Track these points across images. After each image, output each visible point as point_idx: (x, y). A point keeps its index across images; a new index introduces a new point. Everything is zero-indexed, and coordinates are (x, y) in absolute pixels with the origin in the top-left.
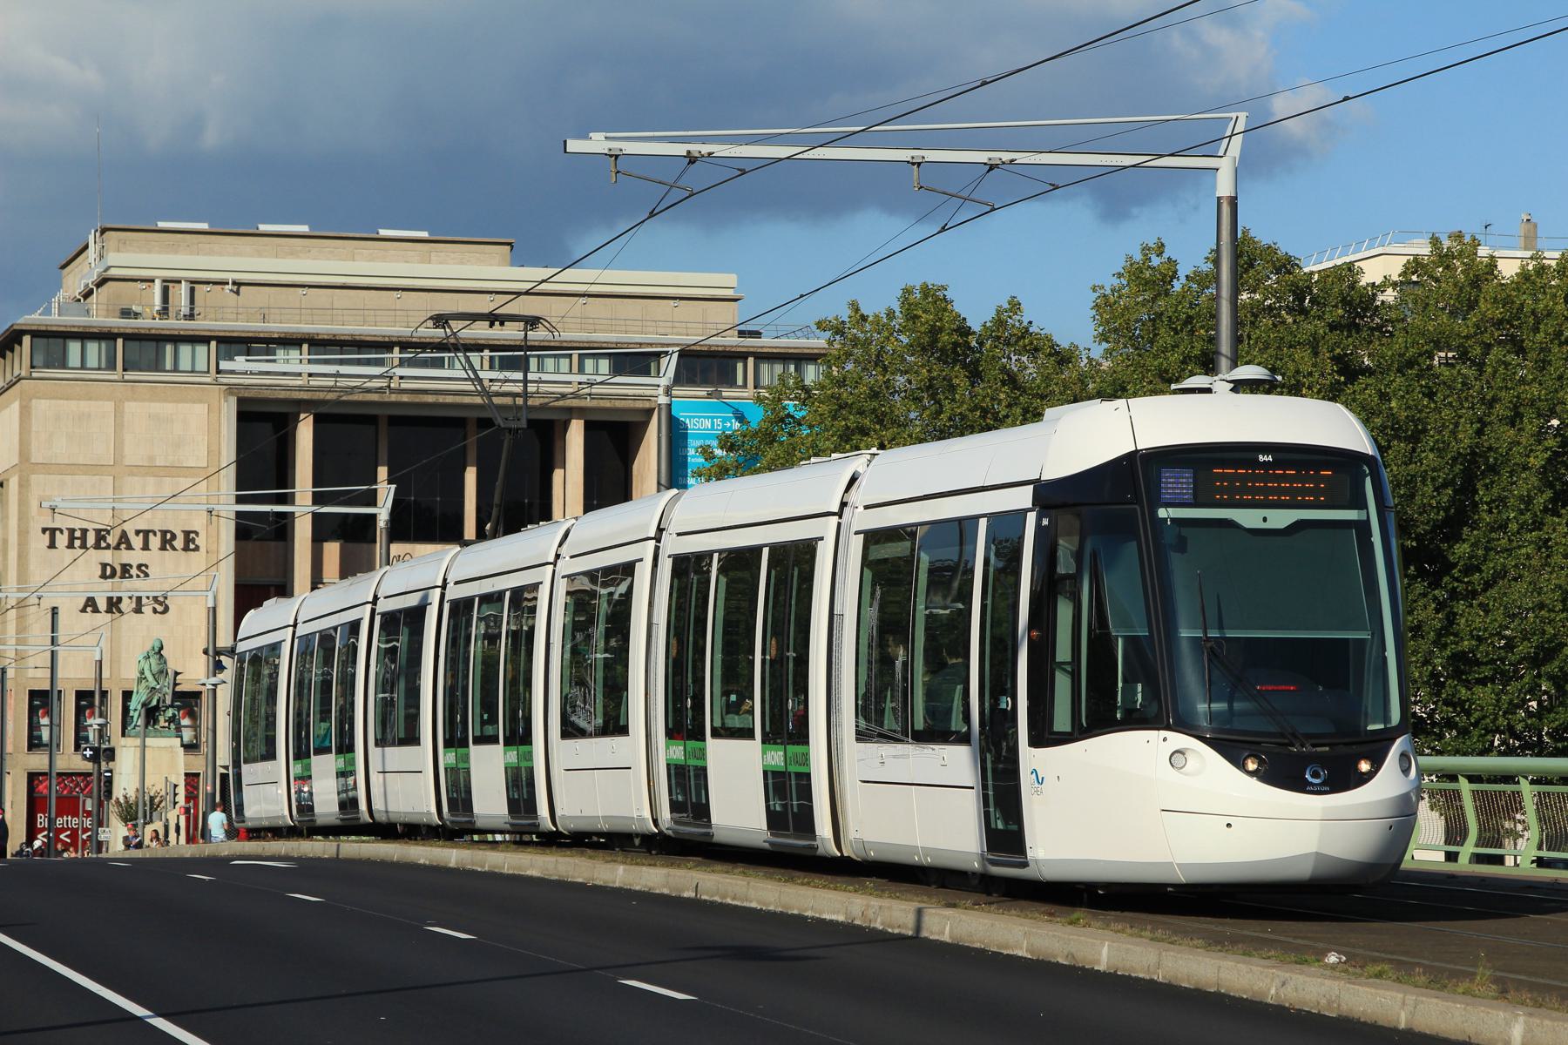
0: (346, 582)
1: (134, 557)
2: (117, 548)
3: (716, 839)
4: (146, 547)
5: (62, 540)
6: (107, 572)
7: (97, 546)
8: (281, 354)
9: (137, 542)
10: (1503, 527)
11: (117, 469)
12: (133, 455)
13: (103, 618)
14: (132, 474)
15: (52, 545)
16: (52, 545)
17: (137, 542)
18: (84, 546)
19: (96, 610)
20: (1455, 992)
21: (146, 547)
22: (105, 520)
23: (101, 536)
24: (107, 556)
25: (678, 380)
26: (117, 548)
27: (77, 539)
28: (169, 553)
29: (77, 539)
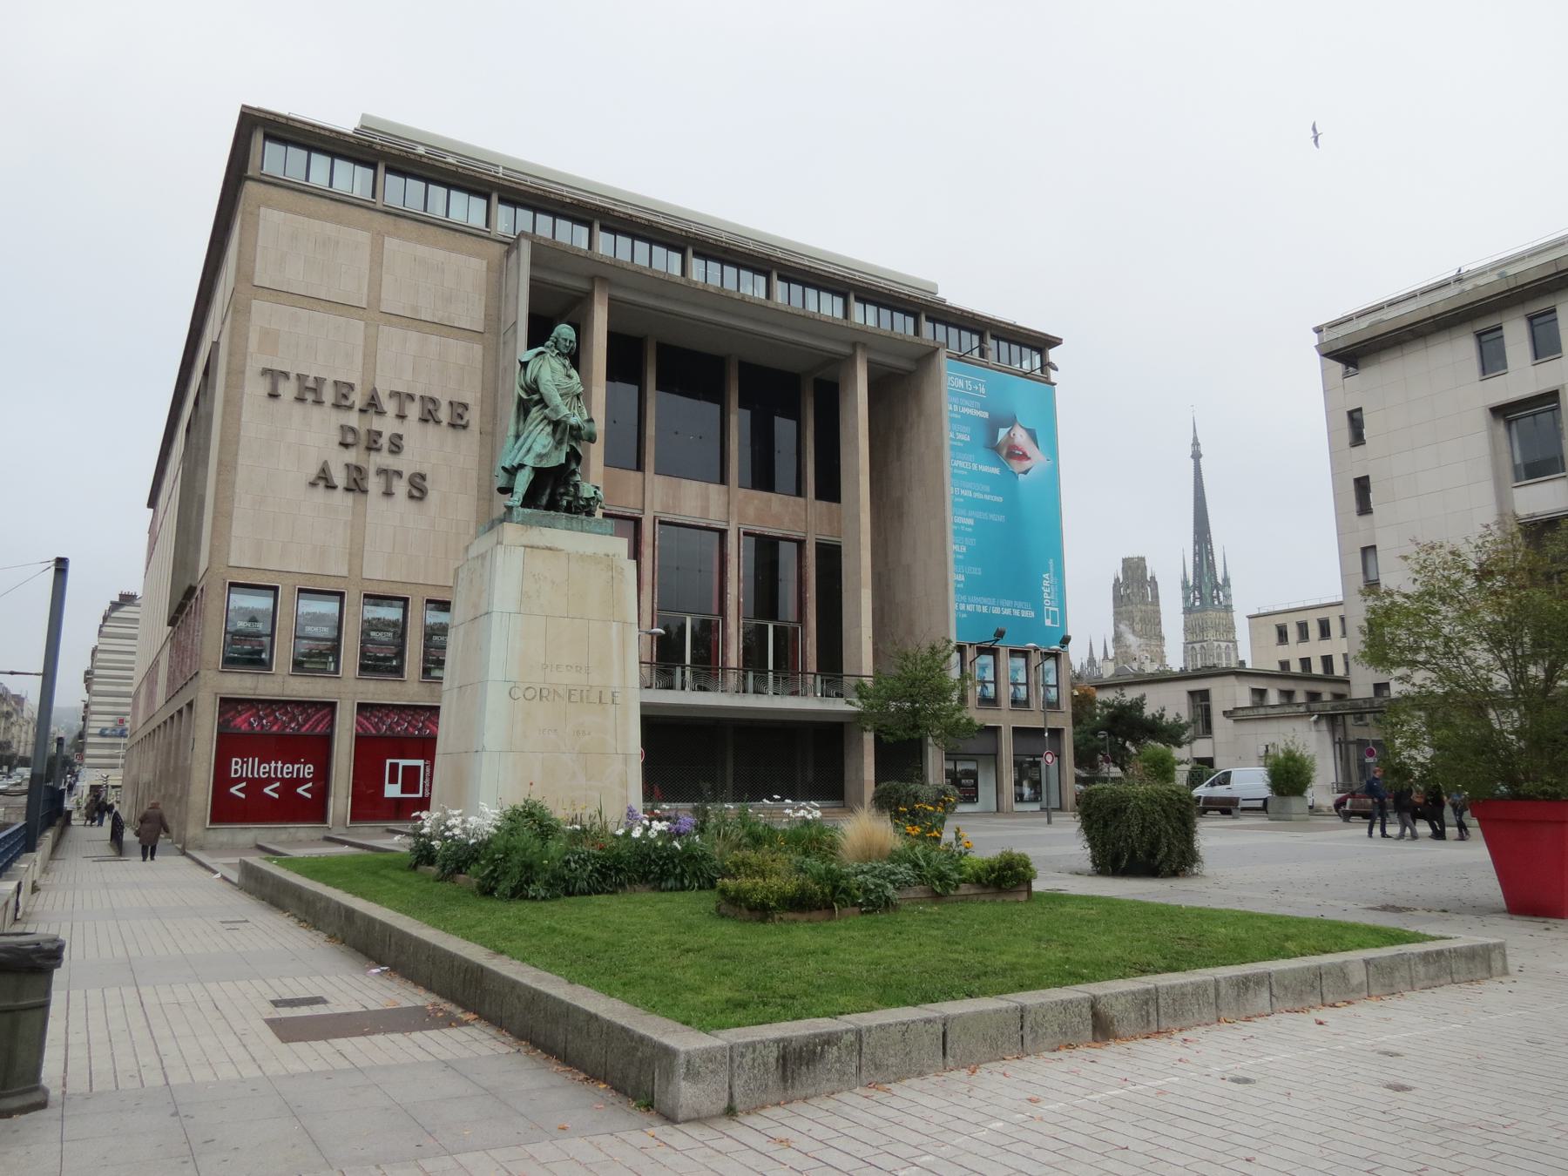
1: (387, 426)
5: (288, 390)
13: (341, 499)
17: (390, 407)
19: (331, 487)
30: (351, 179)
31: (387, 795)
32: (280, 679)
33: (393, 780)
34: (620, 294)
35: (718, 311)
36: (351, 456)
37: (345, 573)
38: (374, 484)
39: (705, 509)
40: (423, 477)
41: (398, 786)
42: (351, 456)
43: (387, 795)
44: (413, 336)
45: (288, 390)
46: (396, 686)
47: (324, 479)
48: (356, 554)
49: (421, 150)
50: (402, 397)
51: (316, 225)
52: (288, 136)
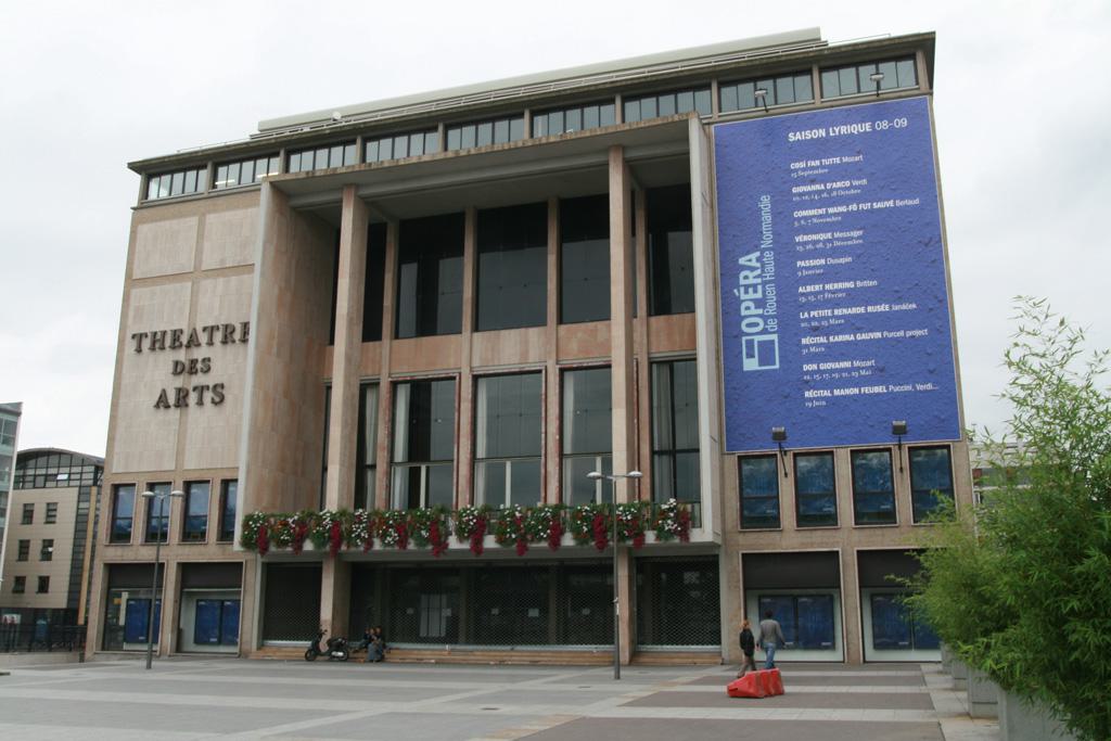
0: (933, 30)
1: (199, 354)
2: (188, 346)
3: (441, 262)
4: (210, 343)
5: (146, 343)
6: (178, 369)
7: (173, 347)
8: (517, 370)
9: (203, 338)
10: (1084, 449)
11: (196, 275)
12: (209, 262)
13: (174, 413)
14: (207, 277)
15: (139, 350)
16: (139, 350)
17: (203, 338)
18: (162, 348)
19: (167, 407)
20: (978, 661)
21: (210, 343)
22: (183, 324)
23: (177, 334)
24: (182, 355)
25: (145, 496)
26: (188, 346)
27: (157, 342)
28: (230, 347)
29: (157, 342)
30: (197, 181)
31: (745, 369)
32: (134, 548)
33: (750, 355)
34: (365, 192)
35: (470, 170)
36: (179, 382)
37: (173, 468)
38: (193, 398)
39: (525, 354)
40: (222, 386)
41: (756, 359)
42: (179, 382)
43: (745, 369)
44: (221, 280)
45: (146, 343)
46: (202, 548)
47: (162, 402)
48: (180, 454)
49: (307, 129)
50: (211, 330)
51: (166, 224)
52: (581, 101)
